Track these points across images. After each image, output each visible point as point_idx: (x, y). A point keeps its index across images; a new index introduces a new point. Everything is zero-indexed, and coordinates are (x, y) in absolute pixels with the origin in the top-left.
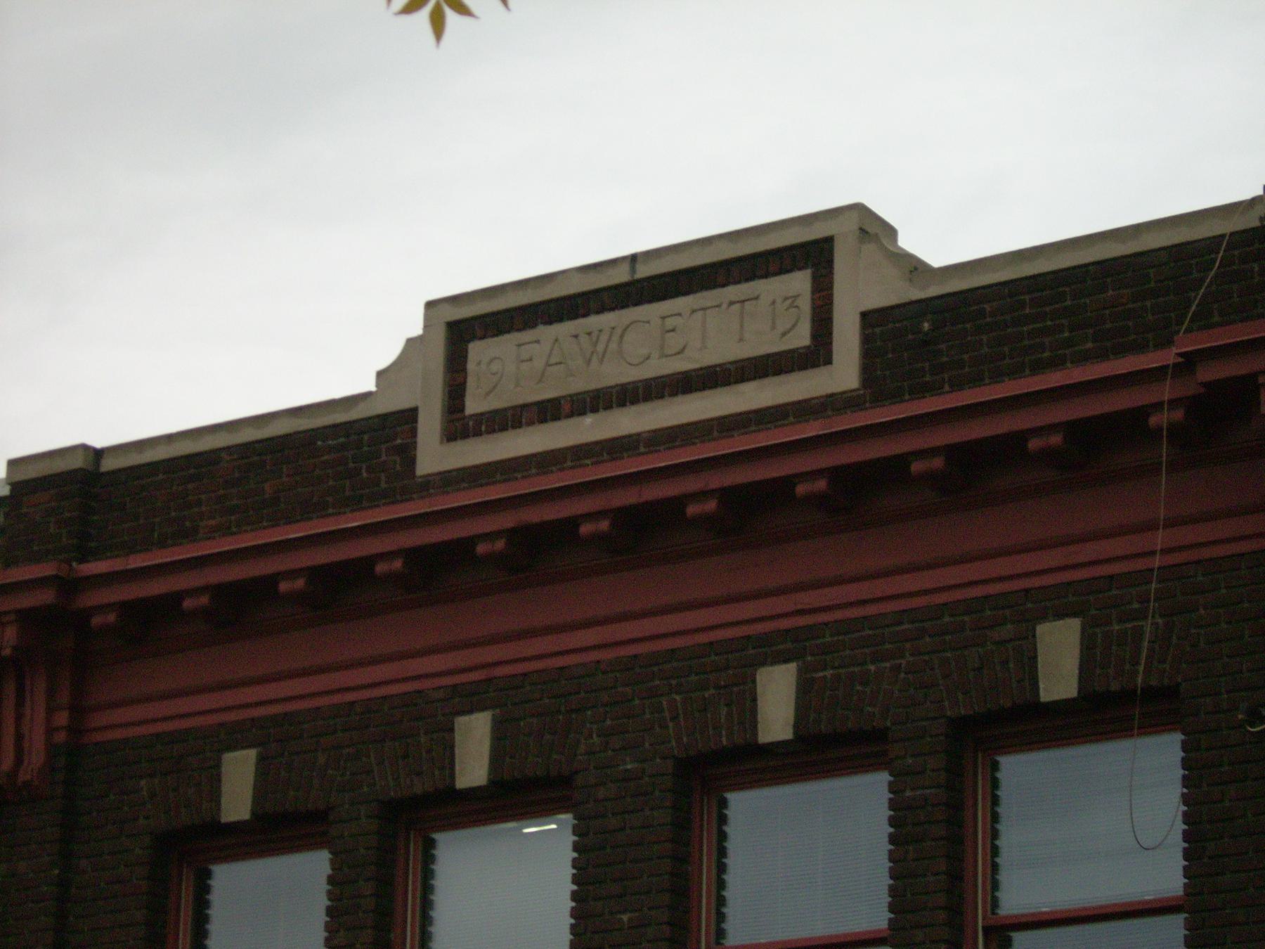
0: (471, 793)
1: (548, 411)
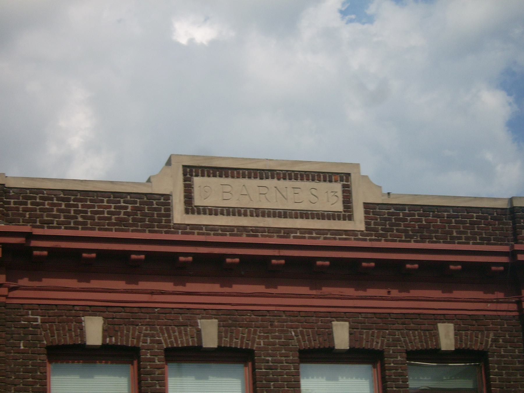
0: (94, 349)
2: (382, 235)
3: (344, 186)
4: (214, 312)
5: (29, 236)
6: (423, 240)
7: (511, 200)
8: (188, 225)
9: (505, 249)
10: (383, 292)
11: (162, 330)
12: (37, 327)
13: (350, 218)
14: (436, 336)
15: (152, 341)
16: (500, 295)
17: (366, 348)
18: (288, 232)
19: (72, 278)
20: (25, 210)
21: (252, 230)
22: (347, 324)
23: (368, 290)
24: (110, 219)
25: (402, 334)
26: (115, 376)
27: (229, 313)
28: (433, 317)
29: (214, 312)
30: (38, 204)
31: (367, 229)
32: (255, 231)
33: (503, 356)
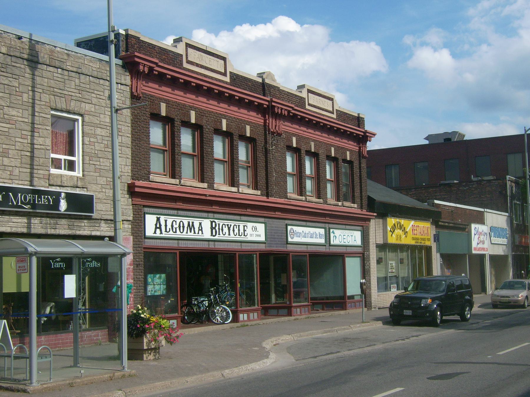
1: (197, 65)
9: (268, 99)
16: (355, 144)
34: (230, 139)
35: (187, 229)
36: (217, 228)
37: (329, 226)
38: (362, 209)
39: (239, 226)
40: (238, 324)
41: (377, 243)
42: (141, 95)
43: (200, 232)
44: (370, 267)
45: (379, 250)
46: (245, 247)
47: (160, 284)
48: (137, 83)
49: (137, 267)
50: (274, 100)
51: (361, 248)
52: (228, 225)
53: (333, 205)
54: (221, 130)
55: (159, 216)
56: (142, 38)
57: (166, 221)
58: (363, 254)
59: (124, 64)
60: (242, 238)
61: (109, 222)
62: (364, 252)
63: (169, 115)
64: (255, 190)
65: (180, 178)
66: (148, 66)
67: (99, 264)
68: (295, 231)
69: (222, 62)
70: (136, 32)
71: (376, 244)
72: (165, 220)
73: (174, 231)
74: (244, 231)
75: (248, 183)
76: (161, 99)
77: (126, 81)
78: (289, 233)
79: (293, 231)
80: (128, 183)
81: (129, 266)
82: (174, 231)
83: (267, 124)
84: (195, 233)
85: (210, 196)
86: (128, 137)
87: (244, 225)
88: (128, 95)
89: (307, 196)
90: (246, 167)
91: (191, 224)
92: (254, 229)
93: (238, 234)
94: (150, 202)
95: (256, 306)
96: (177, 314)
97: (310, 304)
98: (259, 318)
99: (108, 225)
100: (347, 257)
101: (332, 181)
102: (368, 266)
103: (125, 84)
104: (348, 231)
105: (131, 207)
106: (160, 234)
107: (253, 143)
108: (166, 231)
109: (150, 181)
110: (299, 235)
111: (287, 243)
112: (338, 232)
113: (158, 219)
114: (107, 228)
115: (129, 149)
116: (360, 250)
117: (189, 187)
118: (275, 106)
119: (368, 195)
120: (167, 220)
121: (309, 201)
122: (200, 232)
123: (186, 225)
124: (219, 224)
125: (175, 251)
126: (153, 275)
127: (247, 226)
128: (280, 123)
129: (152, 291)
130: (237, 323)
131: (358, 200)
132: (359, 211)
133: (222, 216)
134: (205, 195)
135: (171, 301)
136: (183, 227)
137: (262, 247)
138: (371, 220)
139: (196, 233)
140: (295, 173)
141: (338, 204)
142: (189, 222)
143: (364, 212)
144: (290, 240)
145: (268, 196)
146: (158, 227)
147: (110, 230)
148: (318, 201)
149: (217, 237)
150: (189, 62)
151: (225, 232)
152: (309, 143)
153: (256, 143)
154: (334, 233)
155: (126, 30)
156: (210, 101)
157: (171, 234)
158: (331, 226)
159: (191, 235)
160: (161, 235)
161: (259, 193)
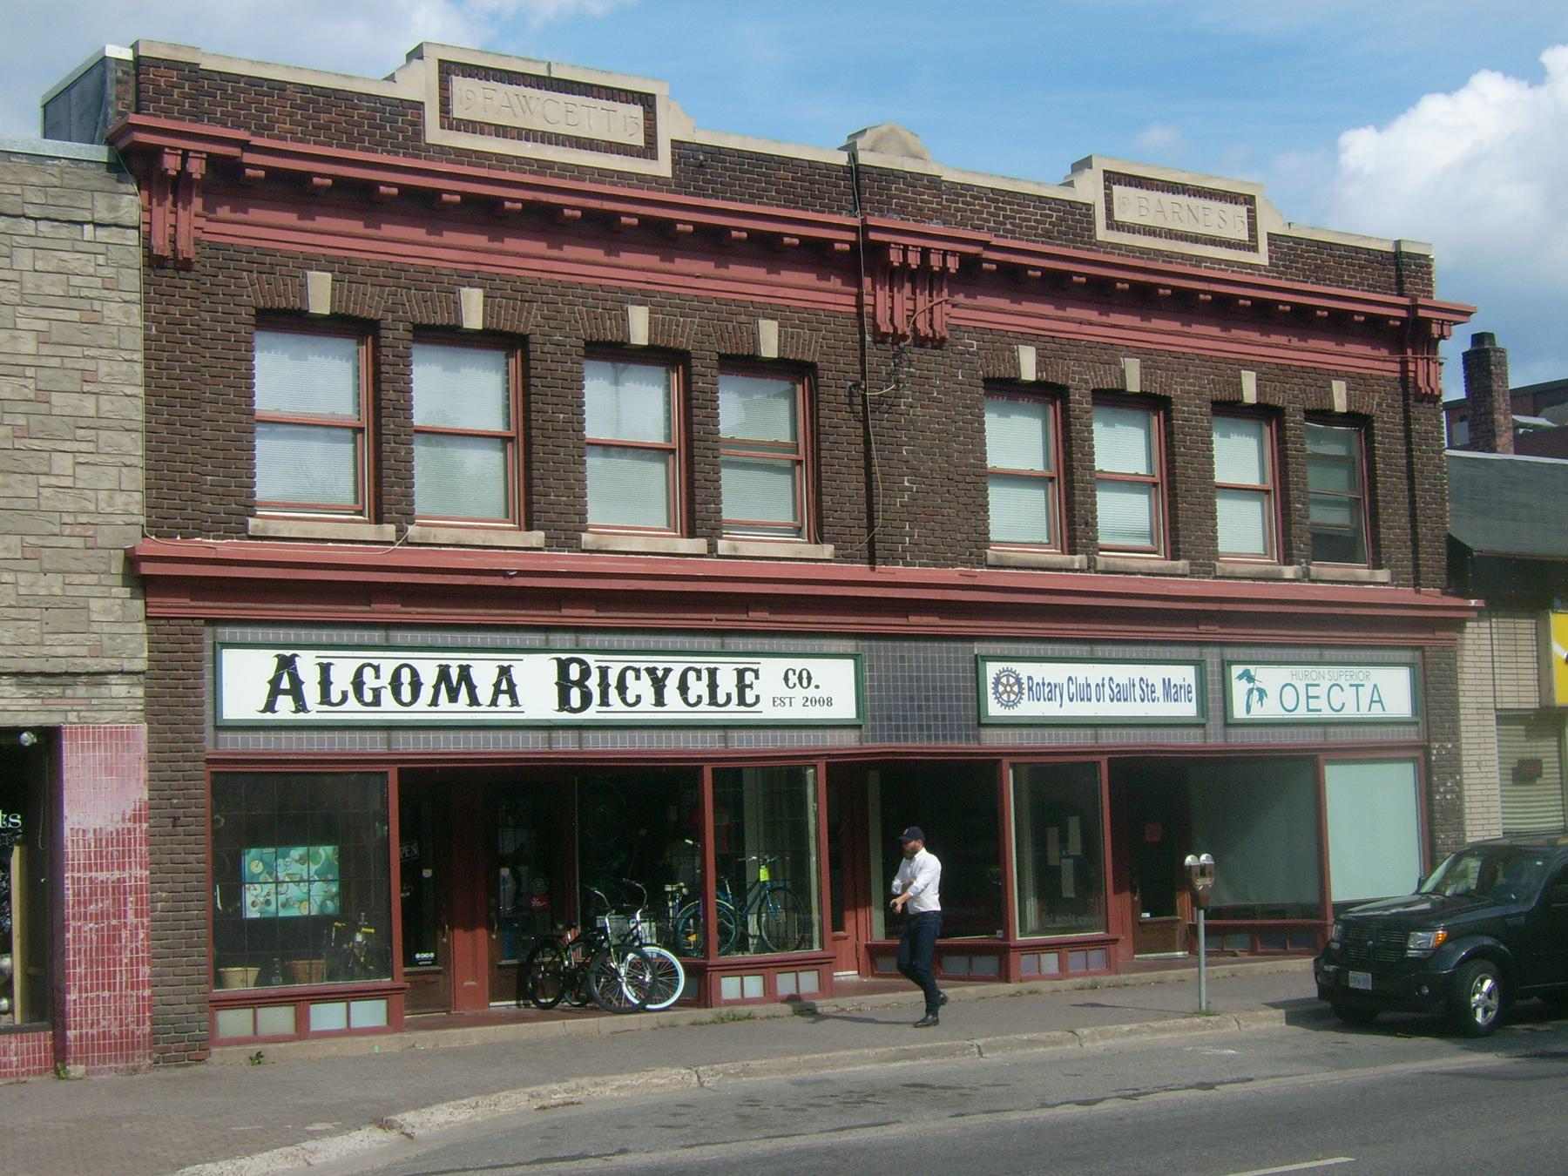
1: (501, 131)
2: (1283, 273)
3: (1249, 211)
4: (1135, 350)
5: (245, 146)
6: (1318, 281)
7: (1398, 243)
8: (1109, 243)
9: (856, 222)
10: (1283, 340)
11: (1088, 366)
12: (971, 354)
13: (654, 157)
14: (1329, 395)
15: (1081, 380)
16: (1384, 352)
17: (340, 313)
18: (1199, 260)
19: (1255, 331)
20: (957, 210)
21: (1167, 256)
22: (1254, 374)
23: (1272, 336)
24: (1037, 229)
25: (1300, 390)
26: (1030, 416)
27: (1148, 352)
28: (1326, 372)
29: (1135, 350)
30: (968, 204)
31: (1270, 264)
32: (1169, 256)
33: (1386, 423)
34: (684, 372)
35: (432, 691)
36: (593, 683)
37: (1222, 655)
38: (1420, 585)
39: (712, 673)
40: (703, 1014)
41: (1499, 706)
42: (946, 334)
43: (504, 700)
44: (1459, 796)
45: (1526, 730)
46: (742, 743)
47: (310, 881)
48: (892, 297)
49: (174, 826)
50: (871, 221)
51: (1413, 729)
52: (651, 672)
53: (1252, 579)
54: (625, 344)
55: (288, 653)
56: (207, 64)
57: (325, 669)
58: (1427, 750)
59: (118, 160)
60: (734, 712)
61: (38, 680)
62: (1429, 741)
63: (1269, 400)
64: (817, 543)
65: (408, 516)
66: (204, 156)
67: (15, 817)
68: (1024, 680)
69: (637, 111)
70: (175, 47)
71: (1496, 710)
72: (320, 664)
73: (368, 697)
74: (742, 687)
75: (795, 519)
76: (628, 292)
77: (119, 214)
78: (990, 686)
79: (1012, 680)
80: (125, 550)
81: (130, 825)
82: (368, 697)
83: (1411, 374)
84: (474, 700)
85: (521, 573)
86: (126, 395)
87: (741, 667)
88: (137, 257)
89: (1101, 550)
90: (788, 464)
91: (454, 674)
92: (793, 679)
93: (706, 699)
94: (533, 616)
95: (816, 948)
96: (389, 979)
97: (400, 984)
98: (395, 1023)
99: (29, 692)
100: (1329, 762)
101: (1268, 492)
102: (1452, 792)
103: (113, 221)
104: (1335, 670)
105: (142, 627)
106: (297, 711)
107: (809, 379)
108: (325, 698)
109: (251, 538)
110: (1171, 691)
111: (981, 722)
112: (1270, 677)
113: (286, 664)
114: (28, 702)
115: (134, 435)
116: (1411, 735)
117: (451, 549)
118: (889, 243)
119: (1449, 535)
120: (716, 669)
121: (1111, 569)
122: (504, 700)
123: (429, 674)
124: (604, 672)
125: (1095, 758)
126: (274, 850)
127: (756, 672)
128: (936, 300)
129: (268, 902)
130: (706, 1007)
131: (1403, 554)
132: (1406, 594)
133: (1383, 656)
134: (503, 573)
135: (366, 935)
136: (416, 685)
137: (847, 741)
138: (1468, 624)
139: (479, 704)
140: (1269, 485)
141: (1073, 562)
142: (448, 667)
143: (1431, 596)
144: (994, 709)
145: (872, 560)
146: (285, 681)
147: (40, 708)
148: (1160, 568)
149: (593, 713)
150: (1113, 225)
151: (639, 697)
152: (1118, 364)
153: (816, 378)
154: (1251, 679)
155: (135, 47)
156: (565, 247)
157: (353, 711)
158: (1229, 653)
159: (459, 710)
160: (301, 716)
161: (827, 550)
